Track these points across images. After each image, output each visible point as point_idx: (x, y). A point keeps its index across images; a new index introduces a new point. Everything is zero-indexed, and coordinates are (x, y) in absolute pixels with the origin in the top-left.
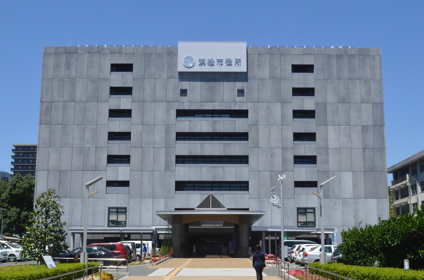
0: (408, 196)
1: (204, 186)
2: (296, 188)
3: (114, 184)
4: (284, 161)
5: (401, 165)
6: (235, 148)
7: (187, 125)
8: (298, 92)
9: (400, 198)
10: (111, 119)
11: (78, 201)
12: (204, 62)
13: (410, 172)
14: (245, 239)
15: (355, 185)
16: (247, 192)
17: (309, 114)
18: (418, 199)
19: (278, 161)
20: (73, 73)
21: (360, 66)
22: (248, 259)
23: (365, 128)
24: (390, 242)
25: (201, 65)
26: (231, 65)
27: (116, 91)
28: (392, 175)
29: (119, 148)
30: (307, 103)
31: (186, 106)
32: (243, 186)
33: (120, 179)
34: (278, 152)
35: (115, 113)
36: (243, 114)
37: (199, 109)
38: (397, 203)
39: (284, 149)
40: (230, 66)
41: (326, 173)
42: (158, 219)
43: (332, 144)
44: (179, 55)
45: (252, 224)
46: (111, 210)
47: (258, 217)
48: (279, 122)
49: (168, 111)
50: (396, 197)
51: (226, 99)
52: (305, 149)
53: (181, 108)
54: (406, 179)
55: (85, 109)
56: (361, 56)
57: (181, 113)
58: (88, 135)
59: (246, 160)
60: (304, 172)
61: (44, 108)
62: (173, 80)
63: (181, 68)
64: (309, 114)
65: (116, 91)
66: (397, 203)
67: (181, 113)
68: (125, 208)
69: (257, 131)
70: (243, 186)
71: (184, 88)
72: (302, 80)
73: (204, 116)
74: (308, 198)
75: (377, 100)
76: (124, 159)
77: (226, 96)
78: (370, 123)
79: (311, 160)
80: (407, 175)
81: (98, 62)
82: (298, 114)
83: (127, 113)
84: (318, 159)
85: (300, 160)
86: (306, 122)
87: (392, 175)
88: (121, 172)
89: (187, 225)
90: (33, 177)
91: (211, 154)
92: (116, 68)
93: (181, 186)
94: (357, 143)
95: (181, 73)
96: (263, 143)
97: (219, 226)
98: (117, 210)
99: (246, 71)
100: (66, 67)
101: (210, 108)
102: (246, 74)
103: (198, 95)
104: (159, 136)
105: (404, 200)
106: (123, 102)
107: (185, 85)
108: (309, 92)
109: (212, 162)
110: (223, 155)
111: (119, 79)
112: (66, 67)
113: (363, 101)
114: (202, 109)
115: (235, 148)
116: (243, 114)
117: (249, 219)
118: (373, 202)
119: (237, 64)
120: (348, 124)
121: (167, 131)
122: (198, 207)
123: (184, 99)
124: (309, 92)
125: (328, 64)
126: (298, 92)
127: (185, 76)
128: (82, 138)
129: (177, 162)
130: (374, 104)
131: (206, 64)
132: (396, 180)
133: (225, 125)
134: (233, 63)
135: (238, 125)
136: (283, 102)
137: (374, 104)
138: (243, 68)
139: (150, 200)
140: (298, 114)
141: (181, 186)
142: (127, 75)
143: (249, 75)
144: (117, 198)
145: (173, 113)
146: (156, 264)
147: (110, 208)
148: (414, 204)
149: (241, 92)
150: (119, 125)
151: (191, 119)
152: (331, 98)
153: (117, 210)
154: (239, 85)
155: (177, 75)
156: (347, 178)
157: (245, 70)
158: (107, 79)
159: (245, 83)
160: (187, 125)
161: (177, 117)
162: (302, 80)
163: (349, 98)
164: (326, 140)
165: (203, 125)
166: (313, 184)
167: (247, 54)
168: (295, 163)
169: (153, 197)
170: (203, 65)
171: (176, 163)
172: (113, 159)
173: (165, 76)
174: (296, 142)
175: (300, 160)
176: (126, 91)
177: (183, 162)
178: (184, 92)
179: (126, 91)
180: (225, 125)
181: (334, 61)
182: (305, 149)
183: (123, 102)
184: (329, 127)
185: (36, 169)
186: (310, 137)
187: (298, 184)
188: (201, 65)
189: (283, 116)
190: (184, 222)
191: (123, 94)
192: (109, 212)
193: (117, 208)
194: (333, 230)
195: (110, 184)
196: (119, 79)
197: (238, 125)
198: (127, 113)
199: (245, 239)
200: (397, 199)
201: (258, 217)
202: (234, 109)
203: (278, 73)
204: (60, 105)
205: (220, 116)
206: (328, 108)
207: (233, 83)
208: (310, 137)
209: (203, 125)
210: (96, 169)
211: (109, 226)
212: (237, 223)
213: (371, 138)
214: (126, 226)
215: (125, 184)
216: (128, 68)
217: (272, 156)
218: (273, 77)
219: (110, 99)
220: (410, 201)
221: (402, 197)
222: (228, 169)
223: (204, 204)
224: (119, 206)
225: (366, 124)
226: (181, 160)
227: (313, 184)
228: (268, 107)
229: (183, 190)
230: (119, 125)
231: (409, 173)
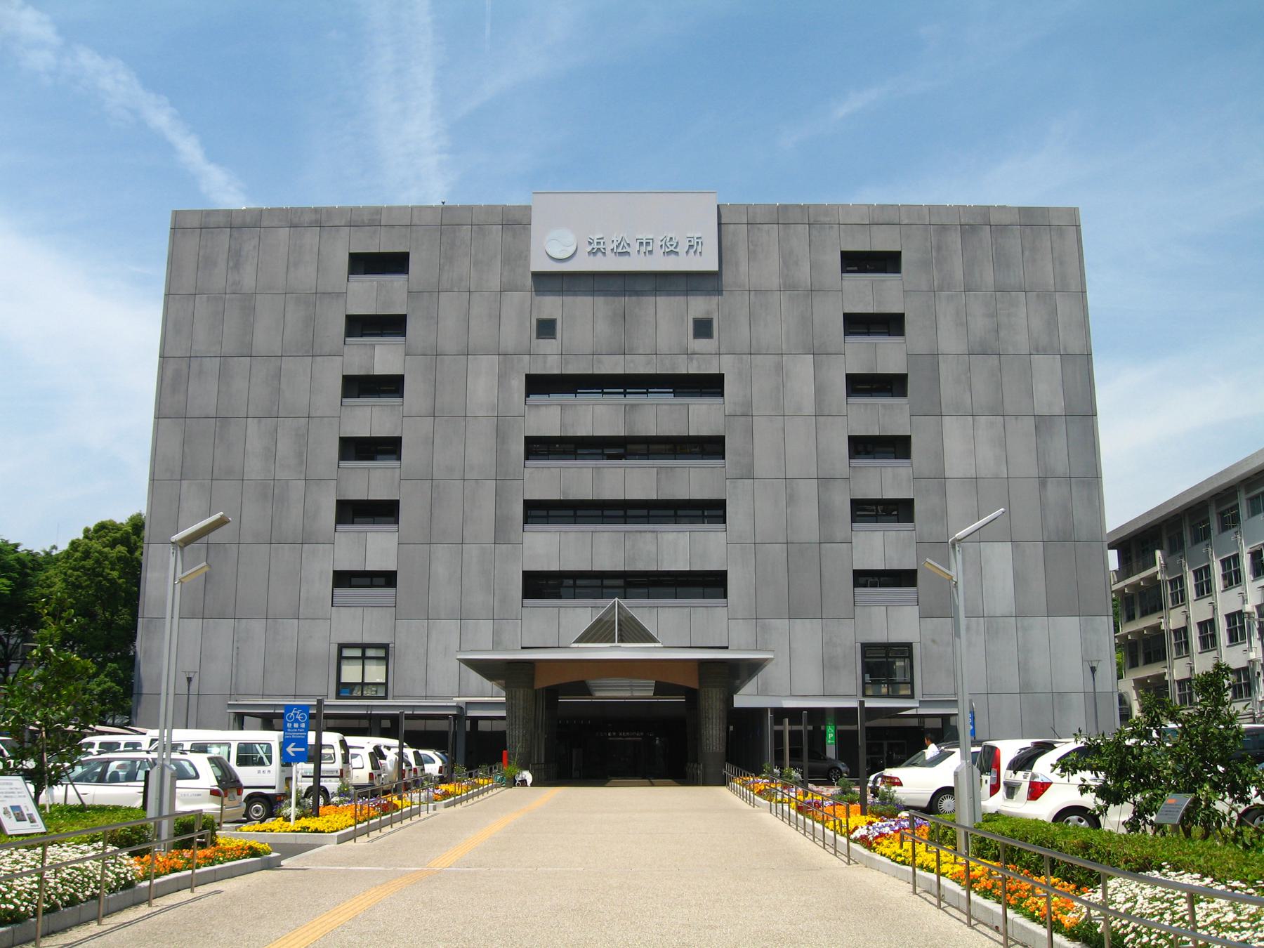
0: (1161, 609)
1: (602, 587)
2: (858, 590)
3: (354, 581)
4: (825, 513)
5: (1141, 524)
6: (690, 479)
7: (551, 417)
8: (857, 324)
9: (1137, 614)
10: (347, 401)
11: (258, 626)
12: (601, 246)
13: (1165, 545)
14: (714, 735)
15: (1020, 579)
16: (721, 601)
17: (892, 385)
18: (1188, 618)
19: (808, 515)
20: (248, 279)
21: (1027, 253)
22: (723, 789)
23: (1043, 423)
24: (1236, 884)
25: (595, 254)
26: (677, 253)
27: (360, 326)
28: (1115, 552)
29: (371, 480)
30: (886, 355)
31: (552, 366)
32: (711, 584)
33: (371, 566)
34: (808, 490)
35: (361, 386)
36: (711, 385)
37: (590, 372)
38: (1128, 629)
39: (824, 481)
40: (673, 256)
41: (945, 548)
42: (475, 678)
43: (956, 465)
44: (533, 227)
45: (736, 690)
46: (346, 653)
47: (750, 668)
48: (809, 407)
49: (502, 378)
50: (1128, 612)
51: (663, 345)
52: (885, 480)
53: (538, 370)
54: (1155, 564)
55: (278, 375)
56: (1028, 230)
57: (538, 385)
58: (285, 447)
59: (720, 513)
60: (879, 546)
61: (169, 373)
62: (516, 296)
63: (540, 264)
64: (892, 385)
65: (360, 326)
66: (1128, 629)
67: (538, 385)
68: (385, 647)
69: (750, 432)
70: (711, 584)
71: (546, 315)
72: (869, 294)
73: (603, 393)
74: (894, 619)
75: (1075, 347)
76: (382, 512)
77: (662, 337)
78: (1058, 408)
79: (898, 510)
80: (1158, 553)
81: (316, 249)
82: (861, 385)
83: (390, 386)
84: (918, 507)
85: (868, 510)
86: (884, 406)
87: (1115, 552)
88: (375, 547)
89: (552, 693)
90: (1141, 661)
91: (619, 496)
92: (364, 263)
93: (540, 585)
94: (1025, 464)
95: (537, 276)
96: (764, 463)
97: (643, 691)
98: (363, 653)
99: (716, 268)
100: (231, 264)
101: (620, 371)
102: (714, 276)
103: (586, 335)
104: (478, 450)
105: (1151, 621)
106: (383, 357)
107: (551, 306)
108: (891, 324)
109: (625, 520)
110: (655, 498)
111: (370, 296)
112: (231, 264)
113: (1038, 350)
114: (596, 372)
115: (690, 479)
116: (711, 385)
117: (734, 673)
118: (1070, 625)
119: (692, 251)
120: (997, 410)
121: (501, 436)
122: (579, 640)
123: (547, 345)
124: (891, 324)
125: (939, 249)
126: (857, 324)
127: (547, 282)
128: (271, 455)
129: (527, 520)
130: (1066, 356)
131: (608, 252)
132: (1127, 566)
133: (659, 415)
134: (682, 249)
135: (699, 416)
136: (819, 353)
137: (1066, 356)
138: (707, 262)
139: (453, 625)
140: (861, 385)
141: (540, 585)
142: (395, 282)
143: (727, 278)
144: (362, 618)
145: (519, 385)
146: (447, 806)
147: (342, 647)
148: (1176, 631)
149: (703, 328)
150: (370, 419)
151: (568, 398)
152: (950, 342)
153: (363, 653)
154: (699, 306)
155: (529, 281)
156: (999, 558)
157: (714, 267)
158: (339, 295)
159: (715, 299)
160: (551, 417)
161: (527, 396)
162: (869, 294)
163: (998, 339)
164: (939, 456)
165: (596, 416)
166: (904, 578)
167: (719, 224)
168: (853, 521)
169: (462, 615)
170: (600, 254)
171: (526, 521)
172: (355, 512)
173: (495, 284)
174: (855, 462)
175: (868, 510)
176: (392, 325)
177: (547, 520)
178: (546, 328)
179: (392, 325)
180: (659, 415)
181: (954, 240)
182: (885, 480)
183: (383, 357)
184: (947, 420)
185: (146, 540)
186: (897, 447)
187: (864, 578)
188: (593, 253)
189: (819, 391)
190: (542, 682)
191: (381, 335)
192: (341, 658)
193: (364, 647)
194: (954, 703)
195: (343, 579)
196: (370, 296)
197: (699, 416)
198: (390, 386)
199: (714, 735)
200: (1131, 618)
201: (750, 668)
202: (685, 372)
203: (803, 273)
204: (212, 365)
205: (647, 393)
206: (943, 367)
207: (682, 299)
208: (897, 447)
209: (596, 416)
210: (306, 539)
211: (338, 697)
212: (693, 684)
213: (1058, 445)
214: (385, 698)
215: (388, 579)
216: (395, 263)
217: (791, 499)
218: (788, 286)
219: (346, 348)
220: (1167, 624)
221: (1144, 614)
222: (670, 537)
223: (592, 635)
224: (367, 639)
225: (1045, 412)
226: (538, 511)
227: (904, 578)
228: (779, 368)
229: (560, 597)
230: (370, 419)
231: (1161, 548)
